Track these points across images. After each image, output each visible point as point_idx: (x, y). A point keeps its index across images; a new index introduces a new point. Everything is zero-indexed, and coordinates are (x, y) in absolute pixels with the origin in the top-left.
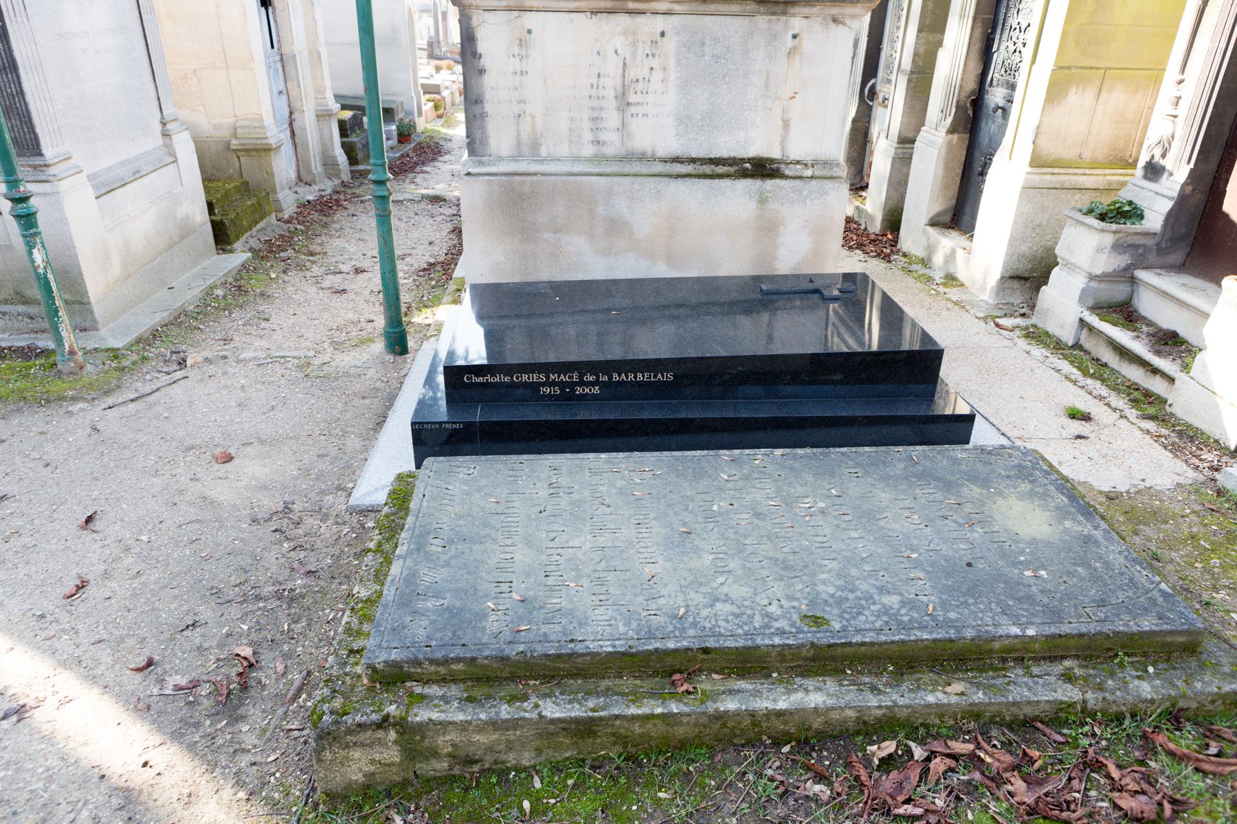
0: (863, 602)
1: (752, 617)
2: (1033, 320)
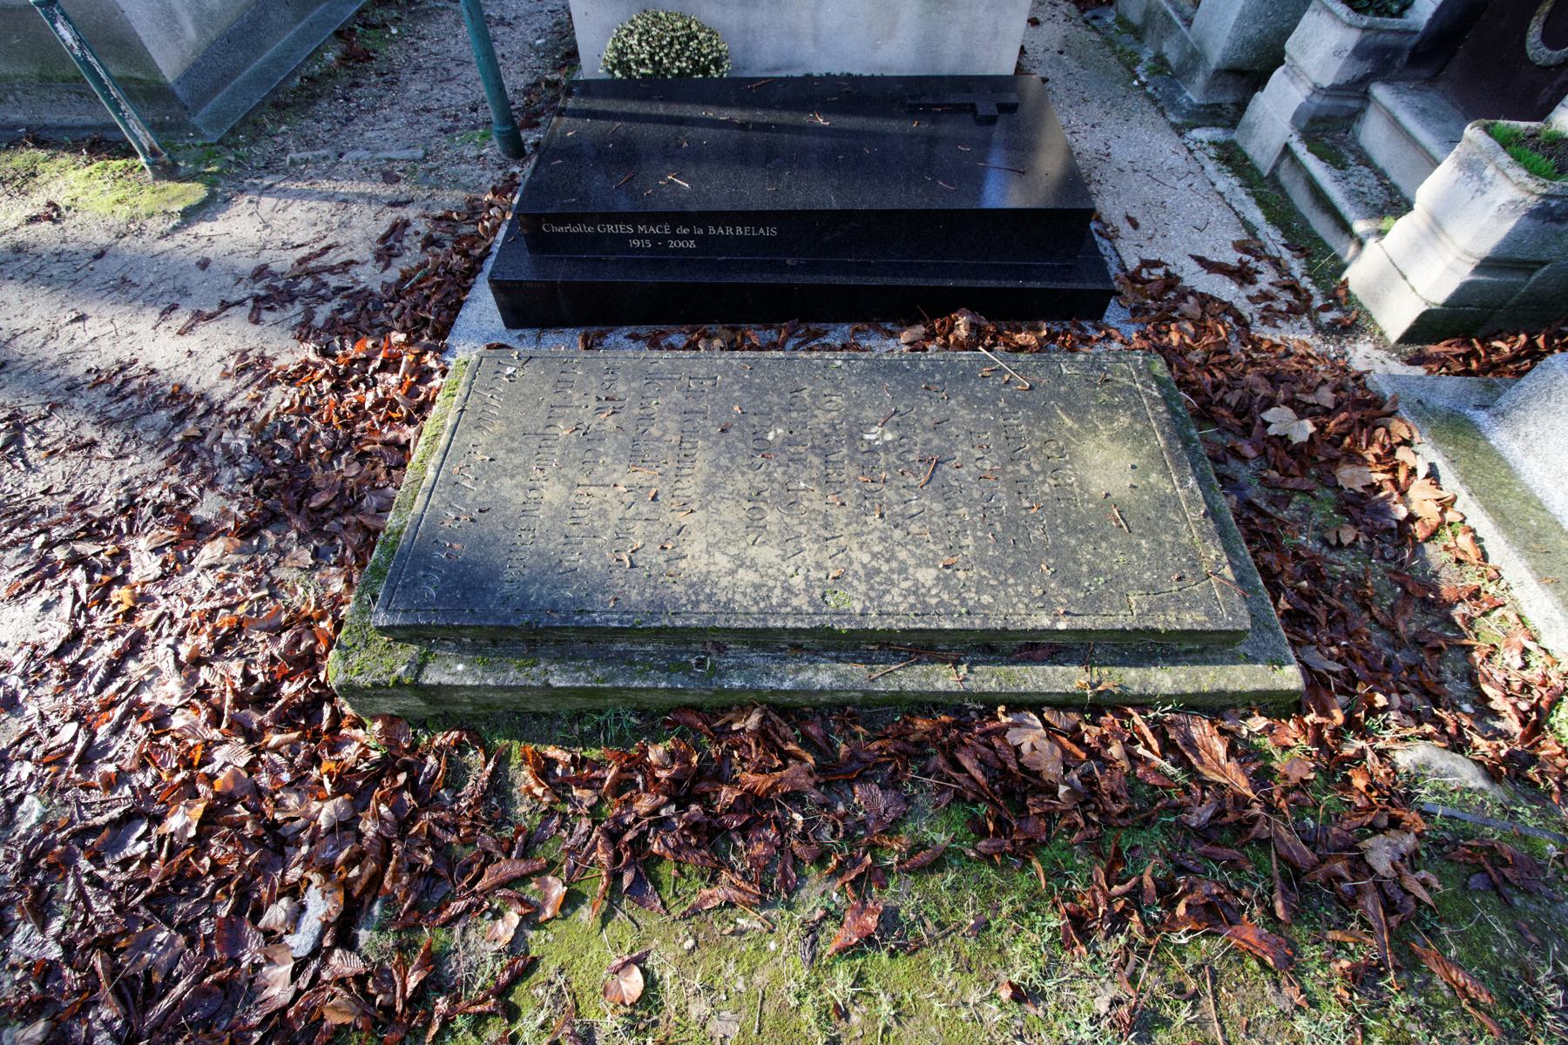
0: (895, 576)
1: (771, 590)
2: (1235, 136)
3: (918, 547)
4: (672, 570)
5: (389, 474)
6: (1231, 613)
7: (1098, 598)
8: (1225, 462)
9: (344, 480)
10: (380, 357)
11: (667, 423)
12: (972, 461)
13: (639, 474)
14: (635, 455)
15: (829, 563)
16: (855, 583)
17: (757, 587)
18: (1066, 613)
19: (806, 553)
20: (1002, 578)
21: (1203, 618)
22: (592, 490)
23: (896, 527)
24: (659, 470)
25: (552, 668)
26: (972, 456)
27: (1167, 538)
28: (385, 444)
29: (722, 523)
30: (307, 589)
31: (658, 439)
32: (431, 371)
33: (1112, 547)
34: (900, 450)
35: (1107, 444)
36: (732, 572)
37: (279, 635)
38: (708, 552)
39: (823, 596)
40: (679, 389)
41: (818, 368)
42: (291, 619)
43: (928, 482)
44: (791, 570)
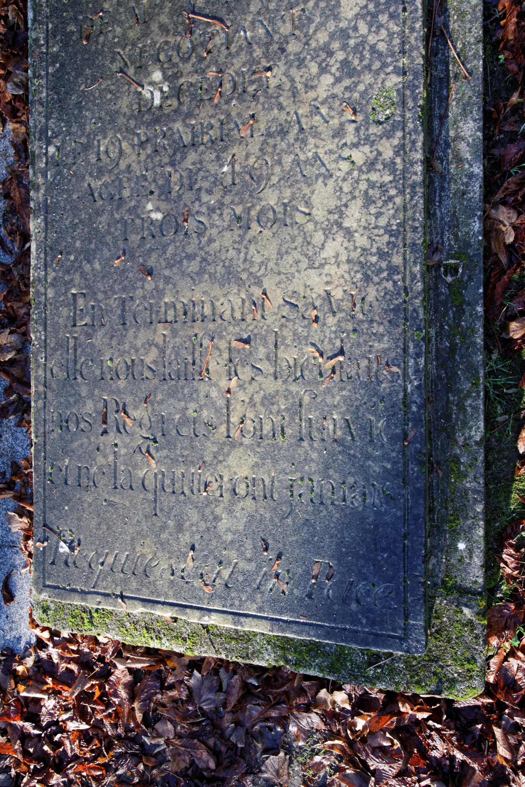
1: (372, 185)
3: (310, 20)
4: (346, 305)
5: (171, 687)
9: (178, 736)
10: (20, 723)
11: (139, 343)
14: (188, 373)
15: (335, 122)
16: (361, 87)
17: (368, 201)
19: (321, 152)
22: (235, 419)
25: (461, 440)
28: (132, 698)
29: (281, 255)
30: (315, 753)
31: (162, 351)
32: (38, 661)
36: (349, 233)
37: (374, 773)
38: (322, 266)
39: (379, 123)
40: (89, 336)
41: (59, 173)
42: (352, 763)
44: (345, 166)
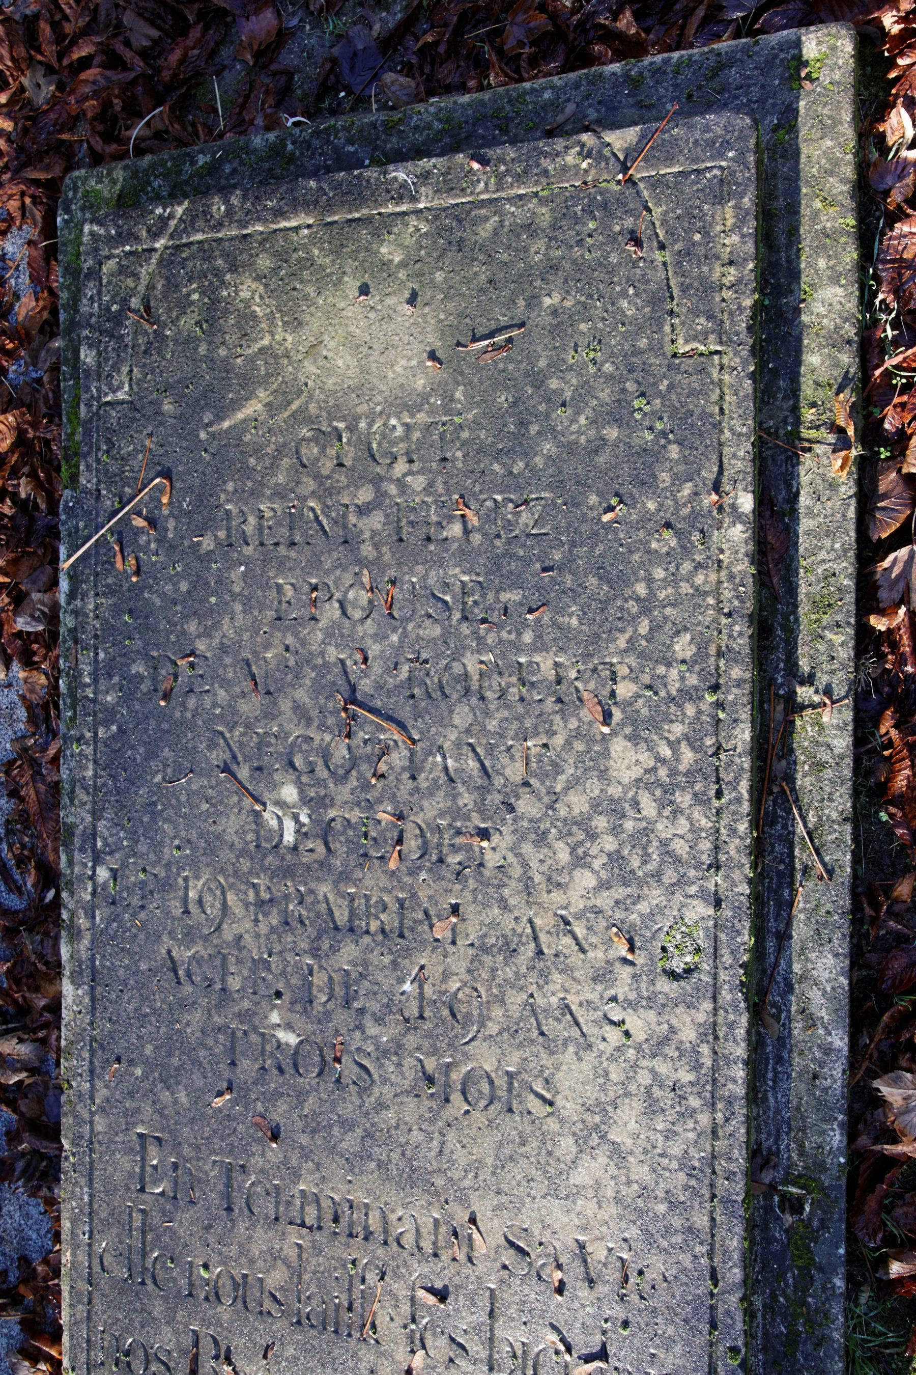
0: (629, 825)
3: (558, 769)
6: (719, 143)
7: (682, 417)
8: (289, 74)
12: (346, 625)
13: (382, 1320)
15: (597, 955)
16: (643, 907)
17: (652, 1108)
18: (717, 487)
19: (573, 1000)
20: (633, 607)
21: (729, 212)
23: (511, 808)
24: (372, 1277)
26: (335, 624)
27: (538, 250)
31: (297, 1273)
33: (557, 367)
34: (322, 772)
35: (307, 335)
36: (617, 1153)
39: (673, 975)
43: (401, 726)
44: (614, 1036)
